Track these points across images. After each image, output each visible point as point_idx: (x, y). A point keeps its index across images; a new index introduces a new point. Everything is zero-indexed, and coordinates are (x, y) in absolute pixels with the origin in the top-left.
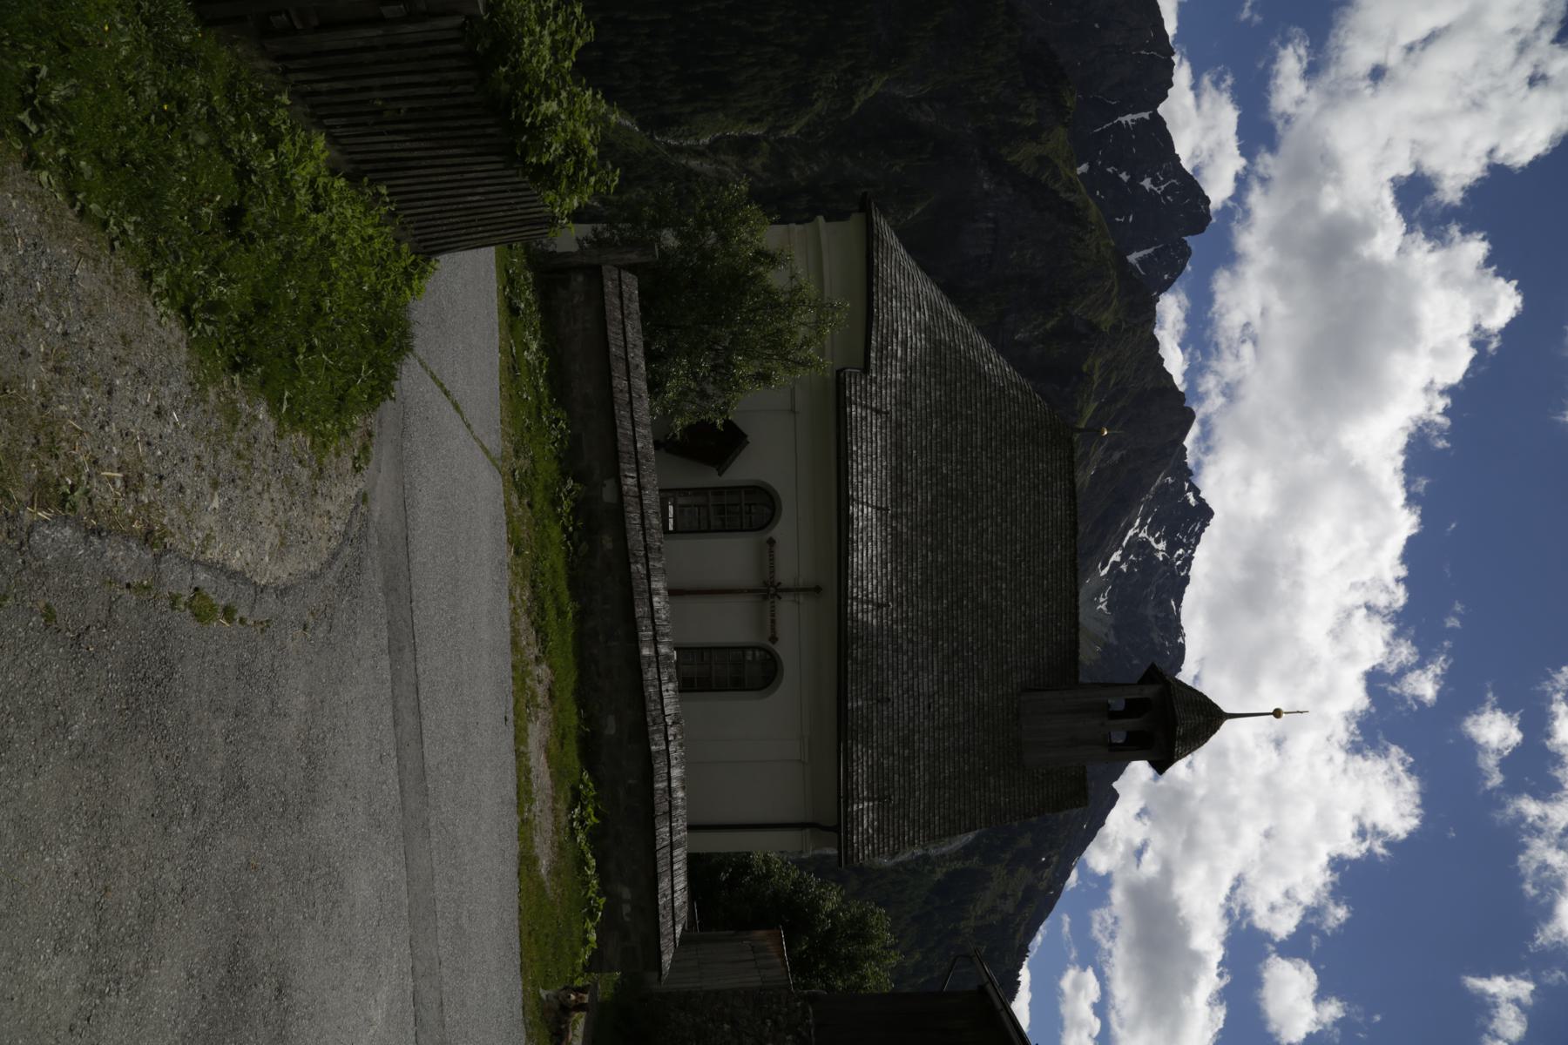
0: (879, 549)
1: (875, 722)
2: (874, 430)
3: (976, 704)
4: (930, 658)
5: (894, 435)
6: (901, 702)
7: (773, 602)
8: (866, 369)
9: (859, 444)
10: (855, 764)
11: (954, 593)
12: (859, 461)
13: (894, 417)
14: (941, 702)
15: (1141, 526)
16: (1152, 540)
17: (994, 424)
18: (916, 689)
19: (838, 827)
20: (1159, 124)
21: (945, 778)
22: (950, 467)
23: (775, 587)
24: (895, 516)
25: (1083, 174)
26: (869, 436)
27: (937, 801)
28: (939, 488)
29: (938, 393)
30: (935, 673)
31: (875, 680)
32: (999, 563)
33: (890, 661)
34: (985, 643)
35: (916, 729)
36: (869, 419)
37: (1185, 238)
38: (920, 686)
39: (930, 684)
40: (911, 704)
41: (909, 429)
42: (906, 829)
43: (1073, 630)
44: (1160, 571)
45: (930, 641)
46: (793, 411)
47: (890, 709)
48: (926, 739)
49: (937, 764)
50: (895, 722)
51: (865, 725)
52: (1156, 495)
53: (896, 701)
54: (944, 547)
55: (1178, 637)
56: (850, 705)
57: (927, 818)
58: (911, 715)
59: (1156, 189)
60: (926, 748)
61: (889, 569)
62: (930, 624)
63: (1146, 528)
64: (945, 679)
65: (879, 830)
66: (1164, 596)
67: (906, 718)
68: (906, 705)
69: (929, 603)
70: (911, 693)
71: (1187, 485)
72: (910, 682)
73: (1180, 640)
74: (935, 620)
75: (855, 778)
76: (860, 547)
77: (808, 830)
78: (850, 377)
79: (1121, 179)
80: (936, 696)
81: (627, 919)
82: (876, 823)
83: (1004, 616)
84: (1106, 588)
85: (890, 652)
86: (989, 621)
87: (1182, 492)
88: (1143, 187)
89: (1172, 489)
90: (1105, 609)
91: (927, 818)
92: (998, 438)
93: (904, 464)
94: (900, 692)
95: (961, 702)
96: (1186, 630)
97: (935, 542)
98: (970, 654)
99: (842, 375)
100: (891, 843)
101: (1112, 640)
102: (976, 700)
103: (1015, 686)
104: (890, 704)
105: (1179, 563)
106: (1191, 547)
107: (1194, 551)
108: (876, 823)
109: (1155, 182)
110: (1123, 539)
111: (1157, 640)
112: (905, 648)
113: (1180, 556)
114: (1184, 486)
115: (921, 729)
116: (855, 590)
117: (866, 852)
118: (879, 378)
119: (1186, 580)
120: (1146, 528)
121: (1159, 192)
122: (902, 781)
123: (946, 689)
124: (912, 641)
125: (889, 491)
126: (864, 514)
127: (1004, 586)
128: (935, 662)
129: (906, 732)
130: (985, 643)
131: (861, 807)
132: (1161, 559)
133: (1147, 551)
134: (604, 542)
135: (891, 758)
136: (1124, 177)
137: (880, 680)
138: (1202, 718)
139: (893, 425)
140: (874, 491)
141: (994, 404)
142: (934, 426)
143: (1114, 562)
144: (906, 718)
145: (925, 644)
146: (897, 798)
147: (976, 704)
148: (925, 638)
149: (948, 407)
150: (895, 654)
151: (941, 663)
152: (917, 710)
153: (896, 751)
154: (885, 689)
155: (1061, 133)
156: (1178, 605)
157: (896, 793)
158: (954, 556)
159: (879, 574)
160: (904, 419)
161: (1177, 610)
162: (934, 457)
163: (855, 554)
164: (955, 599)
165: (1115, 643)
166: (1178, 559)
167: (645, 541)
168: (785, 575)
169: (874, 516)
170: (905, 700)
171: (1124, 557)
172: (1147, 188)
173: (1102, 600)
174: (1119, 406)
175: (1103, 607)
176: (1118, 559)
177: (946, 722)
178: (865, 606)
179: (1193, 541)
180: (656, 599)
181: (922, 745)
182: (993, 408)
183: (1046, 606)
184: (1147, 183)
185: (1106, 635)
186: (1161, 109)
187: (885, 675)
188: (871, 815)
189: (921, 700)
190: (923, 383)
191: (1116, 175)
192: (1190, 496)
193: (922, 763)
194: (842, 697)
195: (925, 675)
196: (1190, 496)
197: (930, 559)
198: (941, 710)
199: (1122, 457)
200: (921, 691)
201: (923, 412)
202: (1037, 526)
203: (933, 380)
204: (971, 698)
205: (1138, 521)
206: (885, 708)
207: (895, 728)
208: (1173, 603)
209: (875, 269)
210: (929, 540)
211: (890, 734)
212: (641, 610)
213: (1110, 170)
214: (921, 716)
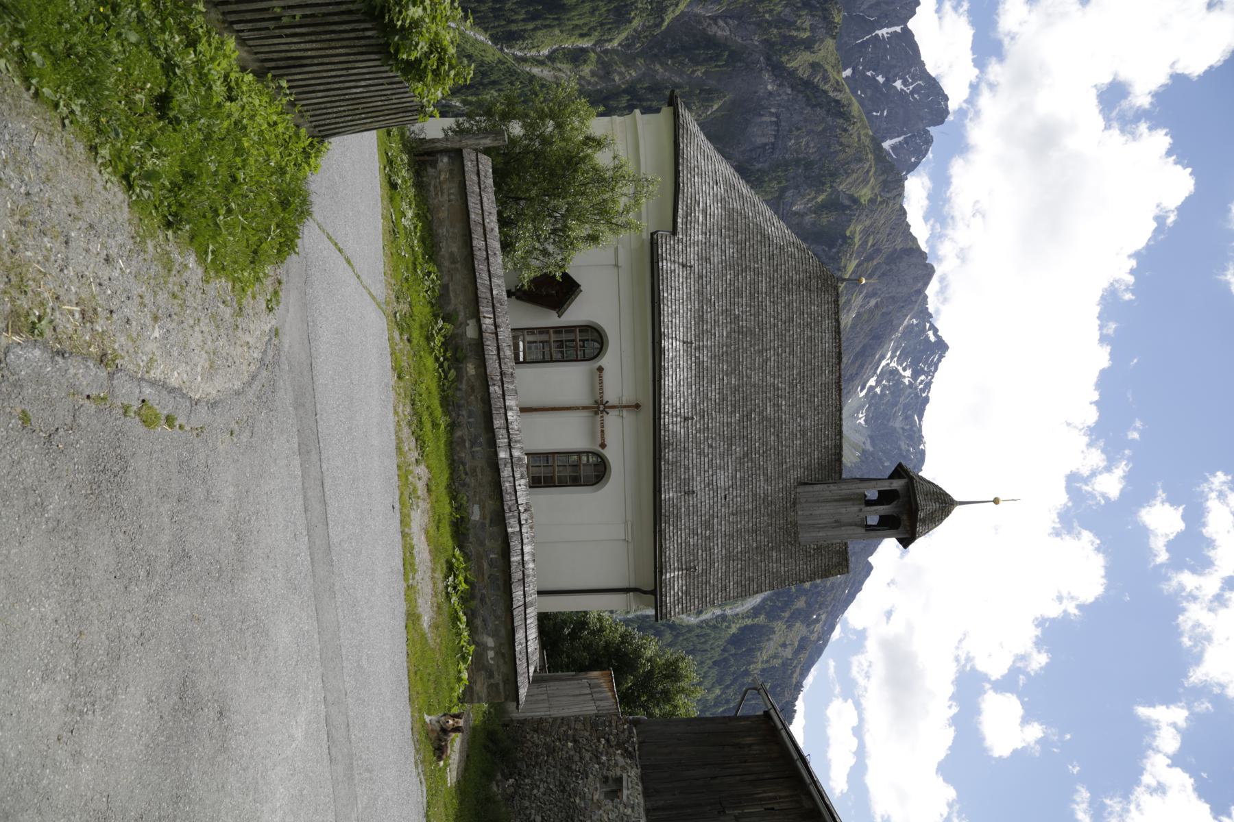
0: (685, 374)
1: (683, 509)
2: (681, 280)
3: (762, 495)
4: (726, 460)
5: (697, 285)
6: (703, 494)
7: (602, 417)
8: (674, 232)
9: (669, 292)
10: (667, 542)
11: (745, 409)
12: (669, 305)
13: (696, 270)
14: (735, 494)
15: (892, 358)
16: (900, 368)
17: (776, 274)
18: (715, 484)
19: (655, 592)
20: (907, 35)
21: (737, 553)
22: (741, 309)
23: (604, 405)
24: (698, 348)
25: (847, 77)
26: (677, 285)
27: (731, 570)
28: (733, 326)
29: (731, 251)
30: (730, 471)
31: (683, 477)
32: (780, 385)
33: (695, 462)
34: (769, 447)
35: (715, 515)
36: (677, 272)
37: (928, 128)
38: (719, 482)
39: (726, 480)
40: (711, 496)
41: (708, 279)
42: (708, 592)
43: (838, 437)
44: (907, 393)
45: (726, 446)
46: (617, 266)
47: (695, 499)
48: (723, 522)
49: (731, 542)
50: (699, 509)
51: (675, 512)
52: (904, 333)
53: (699, 493)
54: (737, 372)
55: (920, 444)
56: (663, 496)
57: (724, 583)
58: (712, 504)
59: (905, 89)
60: (723, 529)
61: (694, 390)
62: (726, 433)
63: (895, 359)
64: (738, 476)
65: (687, 593)
66: (909, 412)
67: (707, 506)
68: (707, 496)
69: (725, 417)
70: (711, 487)
71: (928, 325)
72: (711, 478)
73: (922, 447)
74: (729, 429)
75: (668, 553)
76: (670, 373)
77: (631, 594)
78: (662, 237)
79: (877, 81)
80: (731, 489)
81: (491, 662)
82: (684, 588)
83: (784, 427)
84: (864, 406)
85: (695, 455)
86: (772, 430)
87: (924, 331)
88: (895, 87)
89: (916, 329)
90: (863, 423)
91: (724, 583)
92: (779, 286)
93: (705, 307)
94: (703, 486)
95: (750, 494)
96: (925, 439)
97: (729, 369)
98: (757, 456)
99: (655, 236)
100: (696, 603)
101: (869, 447)
102: (762, 492)
103: (792, 481)
104: (695, 495)
105: (921, 386)
106: (931, 374)
107: (933, 377)
108: (684, 588)
109: (905, 83)
110: (877, 368)
111: (904, 447)
112: (706, 451)
113: (922, 381)
114: (925, 326)
115: (719, 515)
116: (667, 407)
117: (677, 610)
118: (684, 239)
119: (926, 400)
120: (895, 359)
121: (908, 91)
122: (704, 555)
123: (738, 483)
124: (712, 446)
125: (693, 328)
126: (673, 347)
127: (784, 403)
128: (730, 463)
129: (707, 517)
130: (769, 447)
131: (672, 575)
132: (907, 383)
133: (896, 378)
134: (468, 369)
135: (696, 537)
136: (880, 79)
137: (687, 476)
138: (938, 505)
139: (696, 276)
140: (681, 329)
141: (775, 259)
142: (728, 277)
143: (871, 386)
144: (707, 506)
145: (722, 448)
146: (700, 568)
147: (762, 495)
148: (722, 443)
149: (740, 261)
150: (698, 456)
151: (734, 464)
152: (715, 499)
153: (699, 531)
154: (691, 483)
155: (830, 43)
156: (920, 419)
157: (700, 564)
158: (745, 379)
159: (686, 394)
160: (704, 271)
161: (920, 424)
162: (728, 301)
163: (666, 379)
164: (745, 413)
165: (871, 449)
166: (920, 384)
167: (501, 368)
168: (612, 395)
169: (681, 348)
170: (707, 492)
171: (878, 382)
172: (899, 89)
173: (860, 416)
174: (875, 262)
175: (862, 421)
176: (874, 384)
177: (739, 509)
178: (675, 419)
179: (932, 369)
180: (509, 414)
181: (719, 527)
182: (775, 262)
183: (816, 418)
184: (898, 84)
185: (864, 443)
186: (911, 24)
187: (691, 472)
188: (680, 581)
189: (719, 492)
190: (719, 243)
191: (874, 78)
192: (930, 333)
193: (719, 541)
194: (657, 490)
195: (722, 472)
196: (930, 333)
197: (725, 381)
198: (735, 500)
199: (877, 303)
200: (719, 485)
201: (720, 266)
202: (809, 355)
203: (727, 240)
204: (758, 490)
205: (889, 354)
206: (691, 498)
207: (699, 513)
208: (916, 418)
209: (681, 151)
210: (725, 367)
211: (695, 518)
212: (498, 423)
213: (869, 74)
214: (719, 505)
